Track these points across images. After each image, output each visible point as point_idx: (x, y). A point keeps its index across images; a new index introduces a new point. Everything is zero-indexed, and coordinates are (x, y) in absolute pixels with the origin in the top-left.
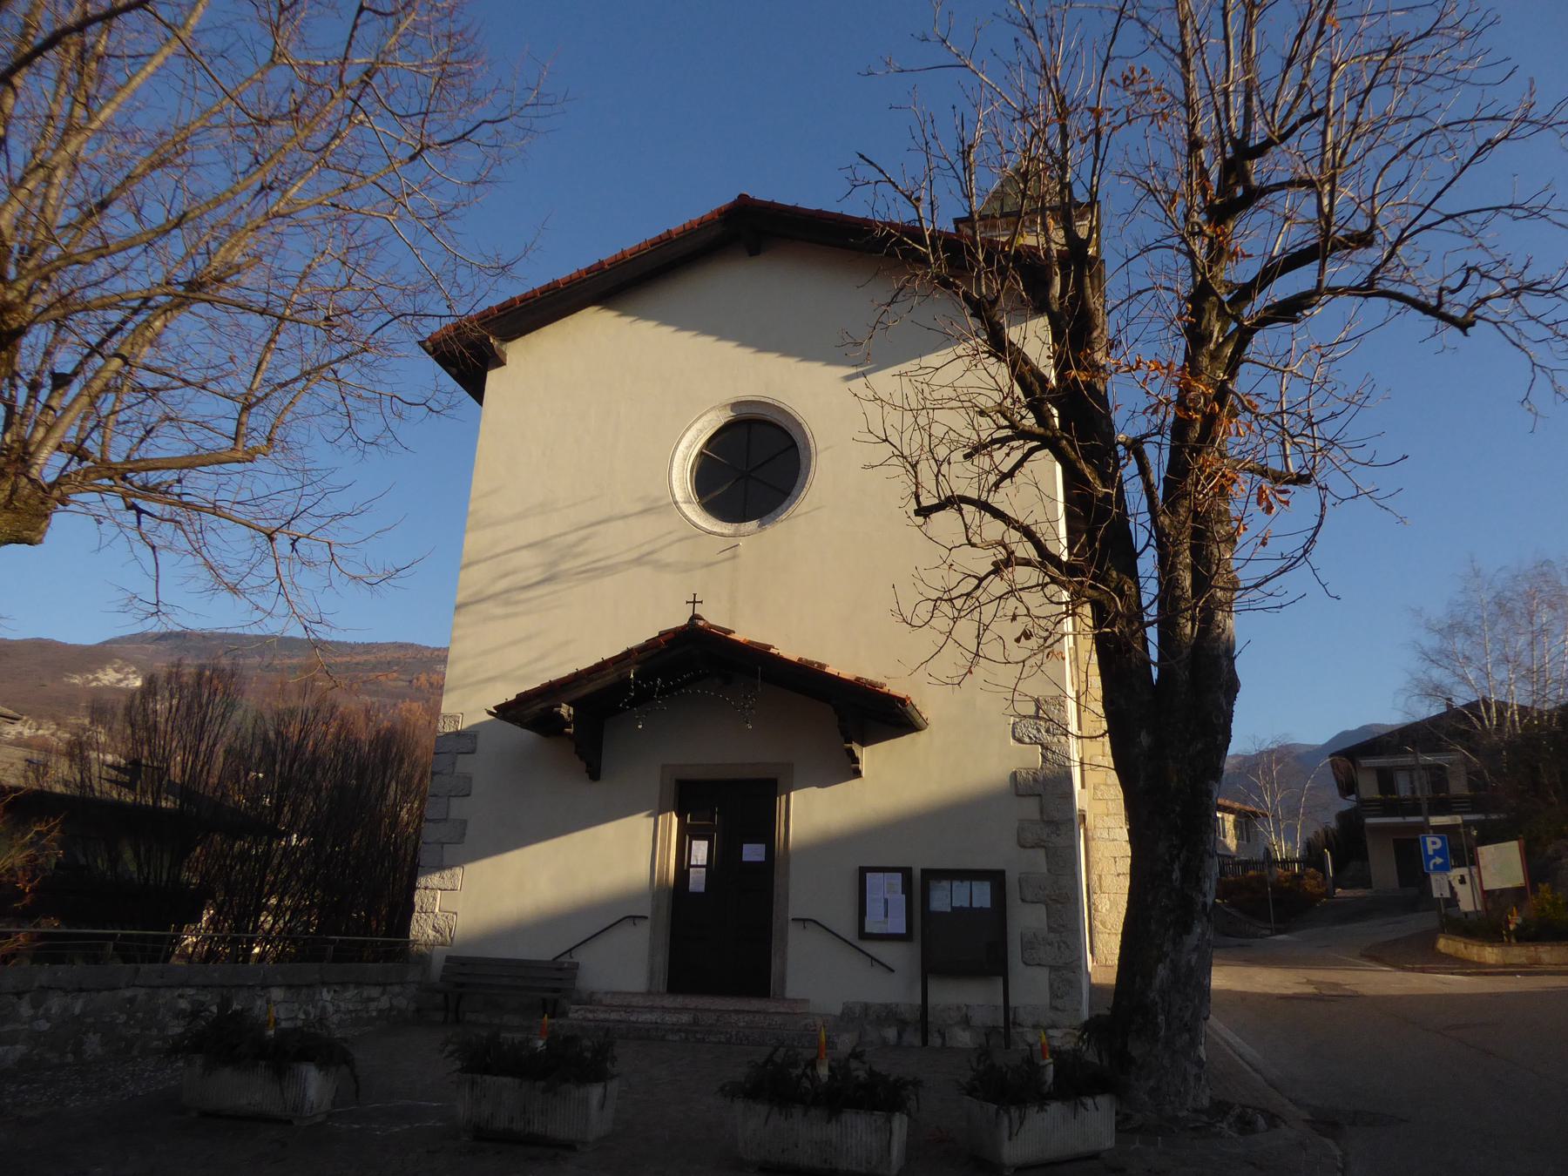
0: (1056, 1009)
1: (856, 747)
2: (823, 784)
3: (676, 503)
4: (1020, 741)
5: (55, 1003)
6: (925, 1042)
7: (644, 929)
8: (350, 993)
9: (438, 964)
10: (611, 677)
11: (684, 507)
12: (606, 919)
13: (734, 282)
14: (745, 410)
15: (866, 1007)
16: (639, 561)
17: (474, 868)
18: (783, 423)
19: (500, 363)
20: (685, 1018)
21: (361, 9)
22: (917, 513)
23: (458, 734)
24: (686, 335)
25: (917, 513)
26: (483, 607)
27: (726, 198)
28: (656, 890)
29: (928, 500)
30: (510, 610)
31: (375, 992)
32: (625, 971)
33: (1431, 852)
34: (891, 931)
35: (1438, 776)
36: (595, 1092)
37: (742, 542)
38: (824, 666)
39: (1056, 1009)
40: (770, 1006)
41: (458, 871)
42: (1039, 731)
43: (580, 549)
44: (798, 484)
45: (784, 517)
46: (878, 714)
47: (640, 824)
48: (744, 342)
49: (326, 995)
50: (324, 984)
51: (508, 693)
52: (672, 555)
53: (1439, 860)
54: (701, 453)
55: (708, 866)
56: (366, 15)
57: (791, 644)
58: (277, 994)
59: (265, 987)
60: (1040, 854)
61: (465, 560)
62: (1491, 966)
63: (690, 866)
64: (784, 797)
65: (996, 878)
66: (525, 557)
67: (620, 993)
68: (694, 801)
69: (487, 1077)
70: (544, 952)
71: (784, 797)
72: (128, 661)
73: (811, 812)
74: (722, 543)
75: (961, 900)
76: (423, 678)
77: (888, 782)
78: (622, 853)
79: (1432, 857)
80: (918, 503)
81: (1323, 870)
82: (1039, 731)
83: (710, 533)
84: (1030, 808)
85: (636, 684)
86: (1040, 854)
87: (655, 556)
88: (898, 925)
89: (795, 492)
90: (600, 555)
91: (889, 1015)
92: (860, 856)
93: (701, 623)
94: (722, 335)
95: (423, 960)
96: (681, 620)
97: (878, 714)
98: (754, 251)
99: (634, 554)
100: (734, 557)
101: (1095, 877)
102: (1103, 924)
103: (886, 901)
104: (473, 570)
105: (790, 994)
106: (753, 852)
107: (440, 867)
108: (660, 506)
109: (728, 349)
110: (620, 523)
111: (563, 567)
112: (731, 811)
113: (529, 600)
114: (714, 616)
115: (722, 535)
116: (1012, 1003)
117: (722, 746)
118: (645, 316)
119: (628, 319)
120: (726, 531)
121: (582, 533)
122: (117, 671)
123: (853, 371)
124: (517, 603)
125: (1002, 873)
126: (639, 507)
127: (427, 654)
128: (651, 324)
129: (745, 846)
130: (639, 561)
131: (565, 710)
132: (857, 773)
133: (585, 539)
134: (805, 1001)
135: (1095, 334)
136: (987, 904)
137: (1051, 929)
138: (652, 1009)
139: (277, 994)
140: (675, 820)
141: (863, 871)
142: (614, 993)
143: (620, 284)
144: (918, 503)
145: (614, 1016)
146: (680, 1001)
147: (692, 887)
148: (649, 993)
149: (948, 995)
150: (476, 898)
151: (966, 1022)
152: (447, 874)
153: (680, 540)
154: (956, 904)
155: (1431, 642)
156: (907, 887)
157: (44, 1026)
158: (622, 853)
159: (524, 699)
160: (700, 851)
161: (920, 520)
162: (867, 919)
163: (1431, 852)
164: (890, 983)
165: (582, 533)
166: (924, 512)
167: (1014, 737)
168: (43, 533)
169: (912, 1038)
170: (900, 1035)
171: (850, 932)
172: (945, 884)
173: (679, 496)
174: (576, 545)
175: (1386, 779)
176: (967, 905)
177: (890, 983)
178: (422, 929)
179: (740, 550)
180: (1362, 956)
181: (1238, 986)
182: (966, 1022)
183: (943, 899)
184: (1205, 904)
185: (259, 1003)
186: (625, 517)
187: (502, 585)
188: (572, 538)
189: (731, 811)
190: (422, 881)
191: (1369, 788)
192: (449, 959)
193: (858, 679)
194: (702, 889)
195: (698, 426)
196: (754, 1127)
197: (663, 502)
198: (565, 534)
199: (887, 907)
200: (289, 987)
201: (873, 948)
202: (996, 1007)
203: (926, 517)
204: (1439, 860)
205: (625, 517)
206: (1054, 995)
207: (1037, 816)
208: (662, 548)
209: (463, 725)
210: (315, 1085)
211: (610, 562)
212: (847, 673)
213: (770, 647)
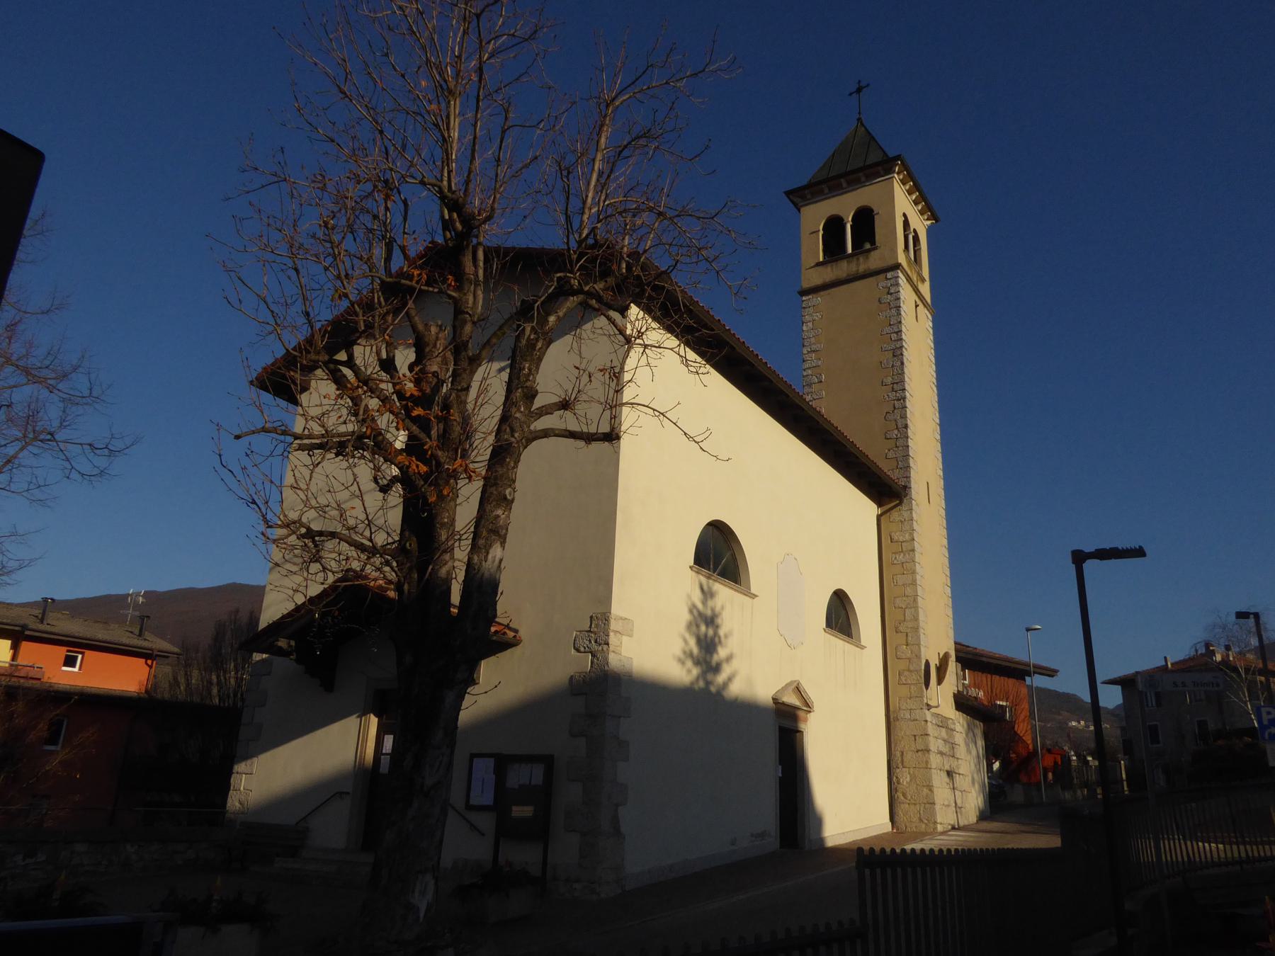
4: (578, 650)
12: (322, 794)
17: (265, 757)
32: (334, 831)
41: (255, 760)
47: (352, 722)
56: (1089, 566)
65: (548, 761)
78: (344, 744)
102: (904, 795)
107: (247, 756)
122: (505, 633)
125: (552, 757)
131: (282, 643)
135: (427, 349)
140: (374, 720)
150: (268, 776)
152: (249, 762)
158: (344, 744)
160: (389, 741)
190: (237, 768)
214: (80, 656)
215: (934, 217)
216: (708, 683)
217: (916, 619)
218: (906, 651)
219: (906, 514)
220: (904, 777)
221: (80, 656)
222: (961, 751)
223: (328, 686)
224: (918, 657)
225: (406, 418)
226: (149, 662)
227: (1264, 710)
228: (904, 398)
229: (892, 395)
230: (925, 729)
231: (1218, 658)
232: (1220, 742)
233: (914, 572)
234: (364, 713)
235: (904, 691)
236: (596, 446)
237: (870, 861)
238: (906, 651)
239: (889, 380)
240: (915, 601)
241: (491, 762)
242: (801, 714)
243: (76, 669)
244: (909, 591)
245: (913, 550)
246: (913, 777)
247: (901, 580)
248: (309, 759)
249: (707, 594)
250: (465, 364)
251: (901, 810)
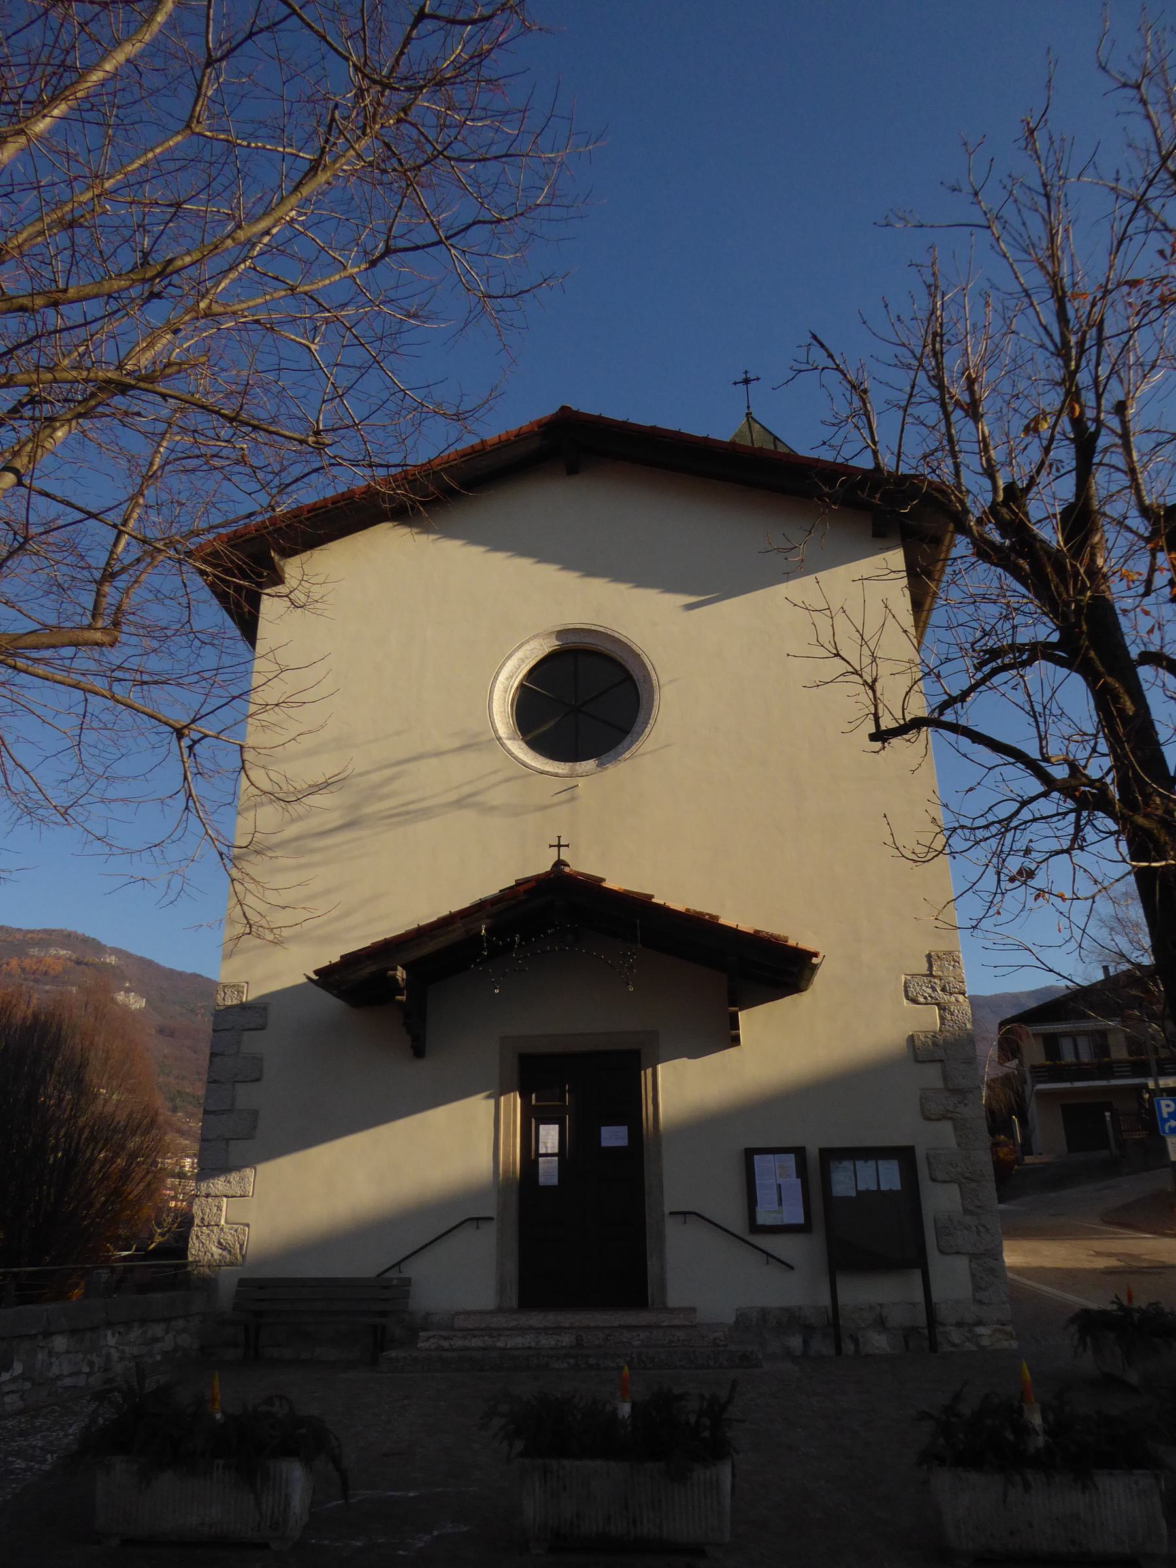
0: (980, 1302)
2: (694, 1054)
3: (499, 739)
4: (914, 1001)
6: (839, 1351)
7: (491, 1229)
8: (135, 1334)
10: (457, 933)
11: (509, 743)
12: (440, 1222)
13: (550, 501)
14: (573, 639)
15: (764, 1313)
16: (460, 803)
17: (268, 1169)
18: (617, 653)
20: (567, 1340)
21: (421, 16)
22: (873, 737)
23: (243, 1007)
24: (499, 556)
25: (873, 737)
27: (548, 410)
28: (501, 1184)
29: (887, 723)
31: (158, 1330)
32: (467, 1283)
33: (1165, 1116)
34: (787, 1221)
35: (1100, 1040)
37: (581, 782)
38: (717, 918)
39: (980, 1302)
40: (643, 1318)
41: (249, 1172)
42: (934, 990)
43: (386, 790)
44: (640, 720)
45: (627, 755)
46: (778, 968)
48: (568, 565)
50: (110, 1324)
51: (332, 955)
52: (497, 797)
54: (521, 686)
55: (561, 1154)
57: (676, 893)
58: (60, 1343)
59: (48, 1335)
60: (948, 1126)
63: (538, 1155)
64: (649, 1071)
65: (905, 1156)
67: (475, 1313)
68: (539, 1079)
69: (566, 1463)
70: (365, 1266)
71: (649, 1071)
73: (682, 1087)
74: (558, 785)
75: (867, 1183)
76: (14, 962)
77: (776, 1046)
78: (454, 1143)
79: (1167, 1120)
80: (878, 725)
81: (1012, 1136)
82: (934, 990)
83: (542, 773)
84: (932, 1075)
85: (488, 941)
86: (948, 1126)
87: (480, 798)
89: (636, 729)
90: (412, 797)
91: (791, 1320)
92: (745, 1135)
93: (567, 869)
94: (542, 557)
95: (208, 1284)
96: (543, 865)
97: (778, 968)
98: (572, 470)
99: (452, 796)
100: (573, 799)
103: (779, 1186)
106: (613, 1136)
108: (479, 742)
109: (550, 573)
110: (434, 761)
111: (368, 810)
112: (589, 1088)
114: (583, 863)
115: (556, 775)
116: (936, 1297)
117: (573, 1012)
118: (450, 534)
119: (432, 537)
120: (560, 771)
121: (387, 773)
123: (693, 599)
126: (457, 743)
127: (19, 936)
128: (458, 543)
129: (603, 1129)
130: (460, 803)
132: (735, 1041)
133: (392, 779)
134: (693, 1310)
136: (896, 1185)
137: (966, 1211)
138: (521, 1330)
139: (60, 1343)
142: (468, 1313)
143: (441, 493)
144: (878, 725)
145: (476, 1342)
146: (536, 1319)
147: (543, 1180)
148: (500, 1310)
149: (863, 1293)
150: (277, 1206)
151: (881, 1323)
152: (234, 1177)
153: (508, 780)
154: (862, 1187)
156: (802, 1170)
158: (454, 1143)
159: (349, 960)
160: (549, 1137)
162: (759, 1209)
163: (1165, 1116)
164: (791, 1283)
165: (387, 773)
166: (881, 736)
167: (907, 997)
169: (821, 1346)
170: (805, 1343)
171: (738, 1225)
172: (847, 1164)
173: (503, 731)
174: (380, 785)
175: (1051, 1043)
176: (874, 1187)
177: (791, 1283)
179: (579, 791)
180: (1107, 1223)
181: (1033, 1261)
182: (881, 1323)
183: (847, 1181)
185: (40, 1356)
186: (438, 754)
188: (375, 777)
189: (589, 1088)
191: (1034, 1053)
192: (242, 1282)
193: (757, 932)
194: (554, 1181)
195: (519, 654)
196: (969, 1504)
197: (484, 738)
198: (368, 772)
199: (781, 1195)
200: (73, 1332)
201: (763, 1241)
202: (914, 1304)
203: (884, 741)
205: (438, 754)
206: (977, 1287)
207: (940, 1084)
208: (488, 789)
209: (250, 996)
211: (425, 804)
212: (746, 926)
213: (652, 896)
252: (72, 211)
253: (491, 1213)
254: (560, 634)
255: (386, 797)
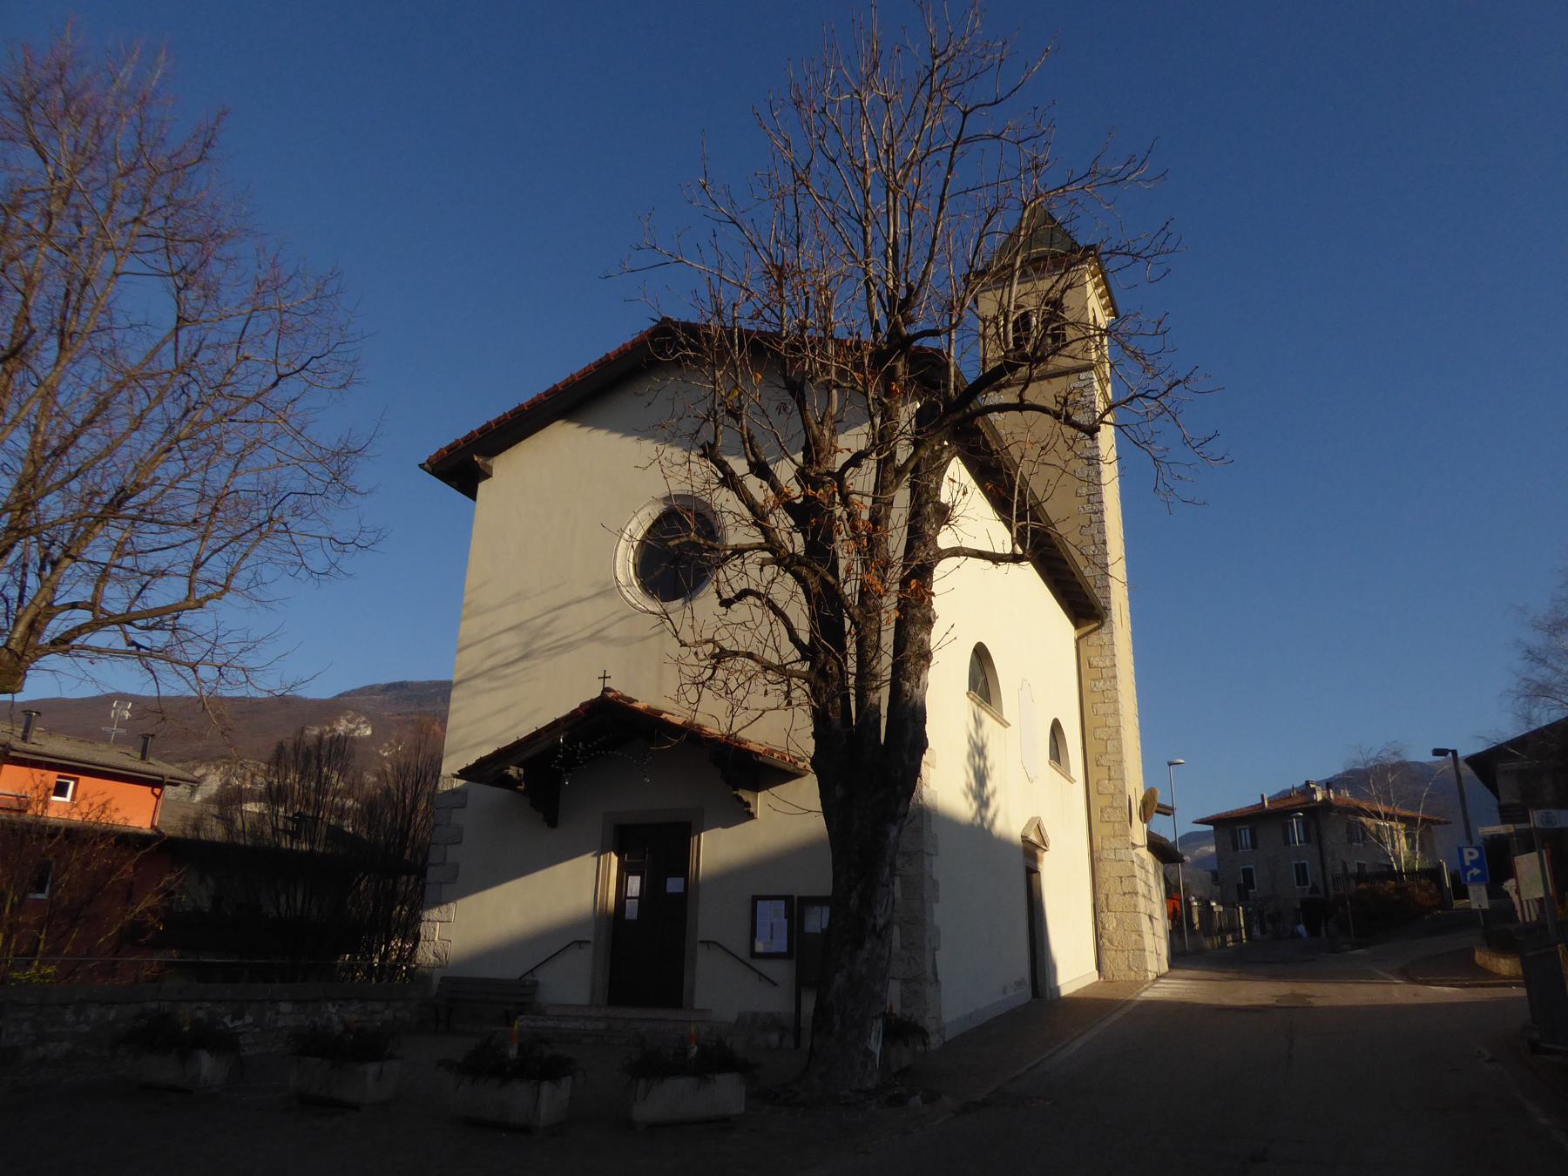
1: (746, 796)
2: (727, 825)
5: (93, 1012)
9: (436, 982)
12: (556, 943)
16: (592, 638)
17: (463, 903)
19: (488, 476)
20: (602, 1025)
26: (473, 683)
30: (495, 684)
31: (378, 1006)
32: (572, 986)
36: (372, 1069)
41: (452, 905)
47: (587, 862)
49: (332, 1009)
52: (613, 632)
53: (1476, 871)
61: (460, 645)
62: (1504, 977)
66: (505, 640)
70: (512, 972)
72: (358, 712)
78: (573, 887)
79: (1470, 868)
88: (781, 945)
93: (611, 695)
96: (596, 693)
99: (587, 633)
101: (1102, 897)
102: (1111, 942)
104: (466, 654)
105: (698, 1005)
106: (674, 885)
107: (439, 903)
108: (609, 589)
111: (535, 646)
112: (656, 849)
113: (505, 677)
114: (619, 685)
117: (648, 795)
118: (598, 426)
124: (505, 677)
126: (593, 591)
128: (603, 432)
130: (592, 638)
131: (513, 771)
132: (751, 816)
139: (285, 1007)
140: (614, 859)
141: (755, 899)
143: (580, 398)
144: (720, 596)
150: (470, 925)
152: (444, 908)
153: (622, 619)
155: (1537, 640)
156: (789, 915)
157: (85, 1028)
158: (573, 887)
159: (482, 762)
160: (634, 884)
161: (724, 609)
165: (546, 618)
168: (22, 684)
170: (781, 1039)
171: (743, 953)
174: (547, 624)
178: (426, 954)
184: (874, 926)
186: (579, 601)
187: (488, 664)
188: (539, 621)
189: (656, 849)
190: (426, 915)
192: (443, 979)
194: (635, 917)
199: (773, 934)
201: (757, 964)
204: (1476, 871)
205: (579, 601)
210: (207, 1065)
211: (573, 639)
213: (661, 712)
214: (72, 784)
215: (1115, 313)
216: (983, 819)
217: (1120, 752)
218: (1109, 787)
219: (1106, 638)
220: (1111, 923)
221: (72, 784)
222: (1154, 892)
223: (552, 822)
224: (1122, 792)
225: (801, 525)
226: (157, 791)
227: (1466, 851)
228: (1102, 512)
229: (1088, 507)
230: (1132, 870)
231: (1319, 797)
232: (1363, 886)
233: (1116, 701)
234: (603, 850)
235: (1106, 829)
236: (1004, 567)
237: (1084, 1007)
238: (1109, 787)
239: (1084, 491)
240: (1118, 732)
241: (781, 905)
242: (1039, 852)
243: (68, 799)
244: (1111, 721)
245: (1115, 677)
246: (1120, 922)
247: (1102, 708)
248: (532, 904)
249: (978, 723)
250: (890, 476)
251: (1108, 956)
252: (50, 394)
253: (591, 938)
254: (667, 499)
255: (550, 634)
